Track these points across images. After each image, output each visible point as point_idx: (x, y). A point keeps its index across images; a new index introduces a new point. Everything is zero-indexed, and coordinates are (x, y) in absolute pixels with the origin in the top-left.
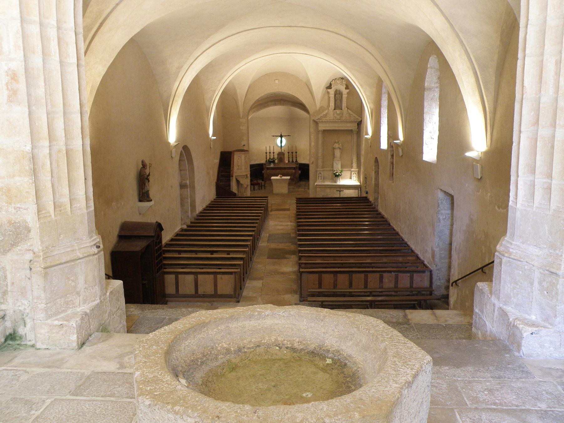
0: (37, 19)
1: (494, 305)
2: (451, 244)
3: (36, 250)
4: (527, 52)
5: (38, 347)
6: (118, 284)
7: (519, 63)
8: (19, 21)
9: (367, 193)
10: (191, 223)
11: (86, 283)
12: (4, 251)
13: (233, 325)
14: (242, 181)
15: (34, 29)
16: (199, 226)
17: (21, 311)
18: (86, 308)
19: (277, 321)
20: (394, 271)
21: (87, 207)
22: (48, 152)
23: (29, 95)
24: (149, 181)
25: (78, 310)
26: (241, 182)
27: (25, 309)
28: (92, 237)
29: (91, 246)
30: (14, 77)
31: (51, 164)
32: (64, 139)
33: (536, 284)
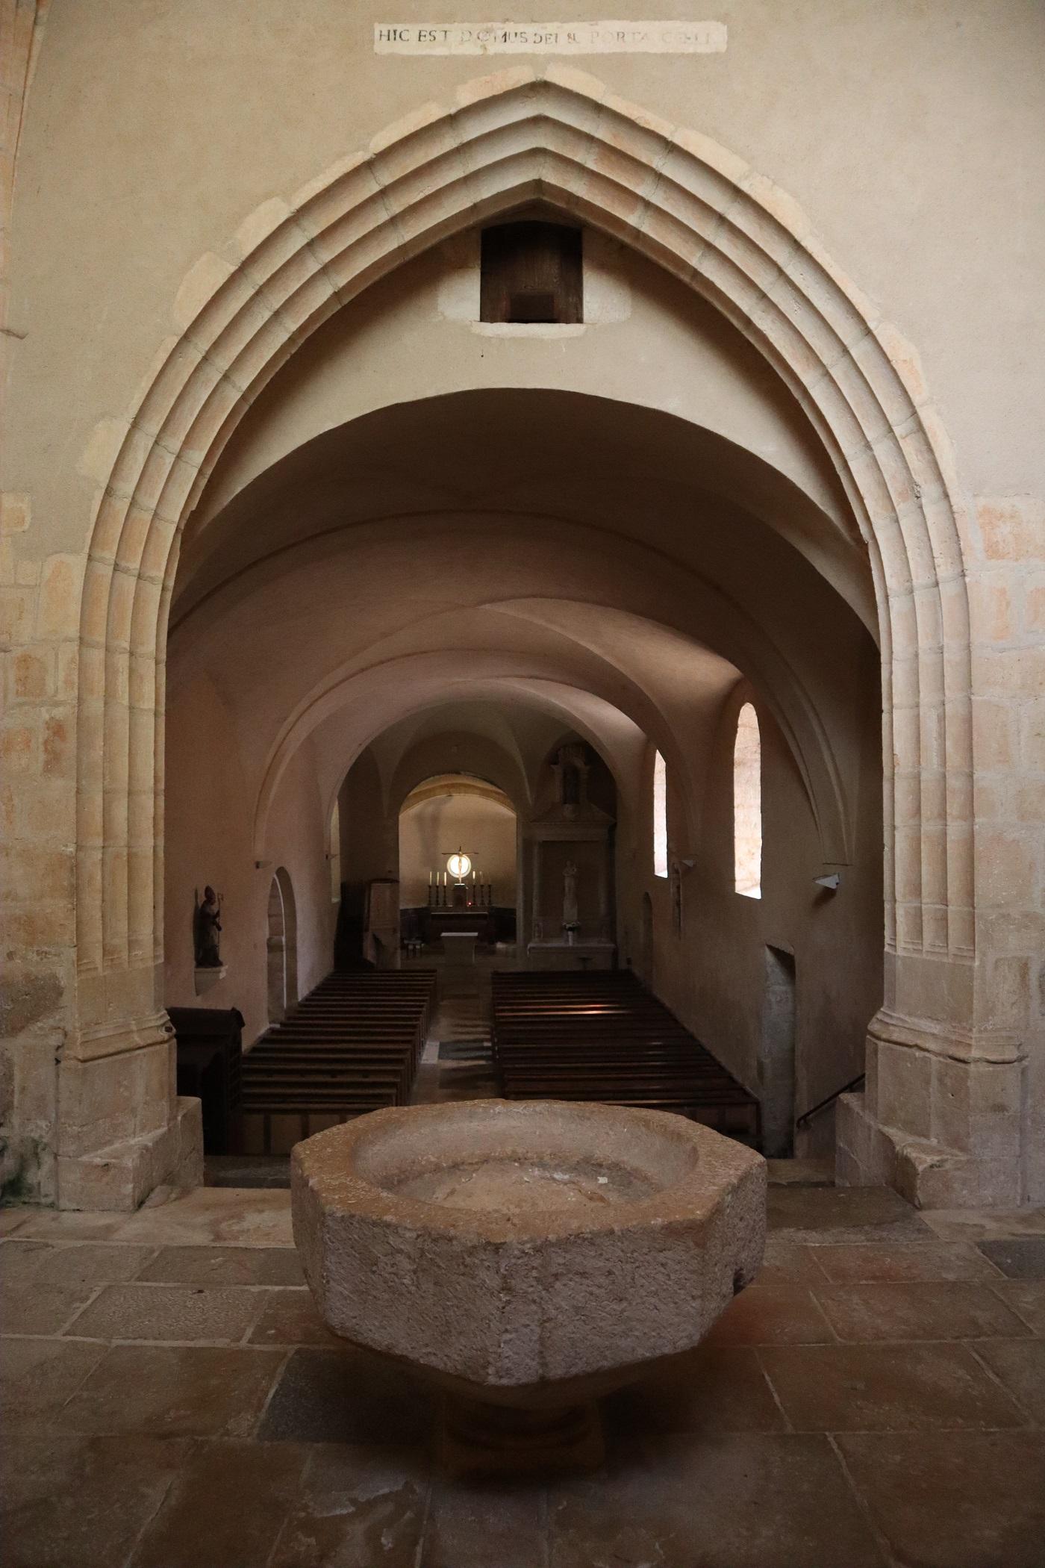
0: (103, 640)
1: (869, 1128)
2: (793, 1050)
3: (69, 1028)
4: (895, 701)
5: (62, 1207)
6: (194, 1102)
7: (885, 717)
8: (77, 643)
9: (629, 961)
10: (289, 1018)
11: (147, 1093)
12: (13, 1029)
13: (444, 1128)
14: (385, 940)
15: (97, 656)
16: (299, 1024)
17: (34, 1140)
18: (147, 1139)
19: (514, 1123)
20: (689, 1105)
21: (156, 957)
22: (100, 856)
23: (79, 761)
24: (220, 929)
25: (132, 1142)
26: (384, 942)
27: (41, 1137)
28: (158, 1011)
29: (158, 1027)
30: (57, 730)
31: (103, 878)
32: (125, 836)
33: (934, 1082)
